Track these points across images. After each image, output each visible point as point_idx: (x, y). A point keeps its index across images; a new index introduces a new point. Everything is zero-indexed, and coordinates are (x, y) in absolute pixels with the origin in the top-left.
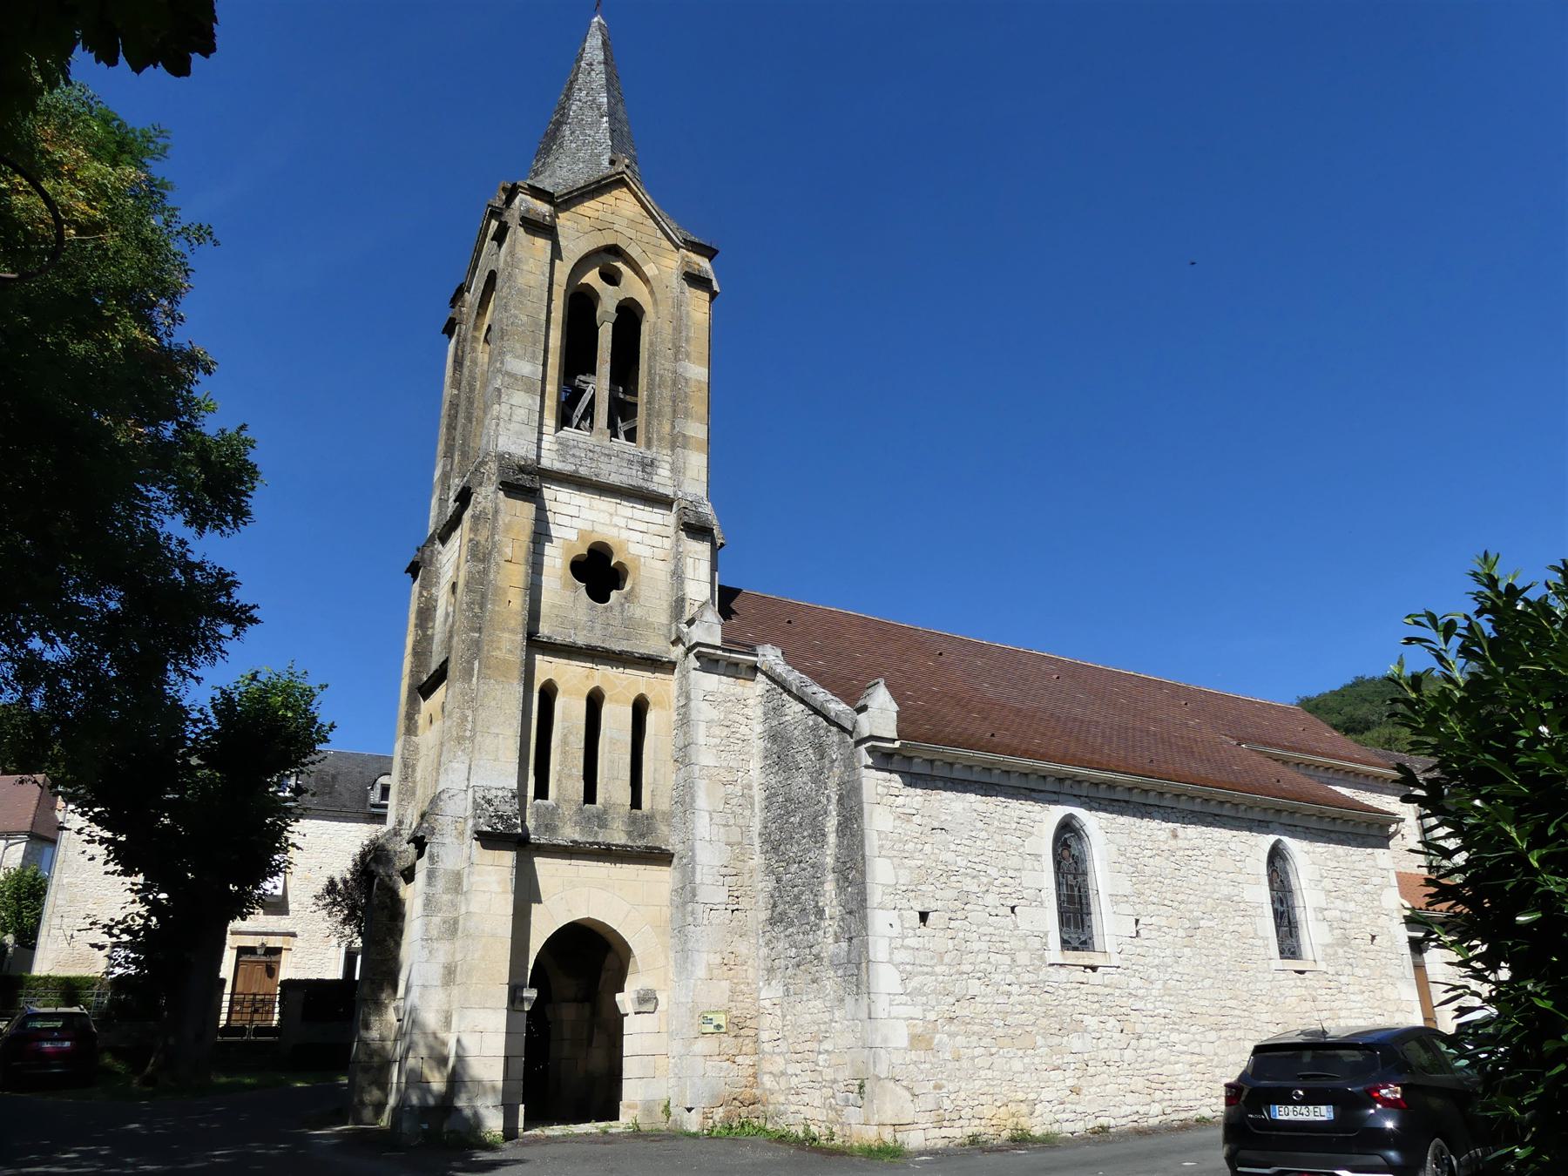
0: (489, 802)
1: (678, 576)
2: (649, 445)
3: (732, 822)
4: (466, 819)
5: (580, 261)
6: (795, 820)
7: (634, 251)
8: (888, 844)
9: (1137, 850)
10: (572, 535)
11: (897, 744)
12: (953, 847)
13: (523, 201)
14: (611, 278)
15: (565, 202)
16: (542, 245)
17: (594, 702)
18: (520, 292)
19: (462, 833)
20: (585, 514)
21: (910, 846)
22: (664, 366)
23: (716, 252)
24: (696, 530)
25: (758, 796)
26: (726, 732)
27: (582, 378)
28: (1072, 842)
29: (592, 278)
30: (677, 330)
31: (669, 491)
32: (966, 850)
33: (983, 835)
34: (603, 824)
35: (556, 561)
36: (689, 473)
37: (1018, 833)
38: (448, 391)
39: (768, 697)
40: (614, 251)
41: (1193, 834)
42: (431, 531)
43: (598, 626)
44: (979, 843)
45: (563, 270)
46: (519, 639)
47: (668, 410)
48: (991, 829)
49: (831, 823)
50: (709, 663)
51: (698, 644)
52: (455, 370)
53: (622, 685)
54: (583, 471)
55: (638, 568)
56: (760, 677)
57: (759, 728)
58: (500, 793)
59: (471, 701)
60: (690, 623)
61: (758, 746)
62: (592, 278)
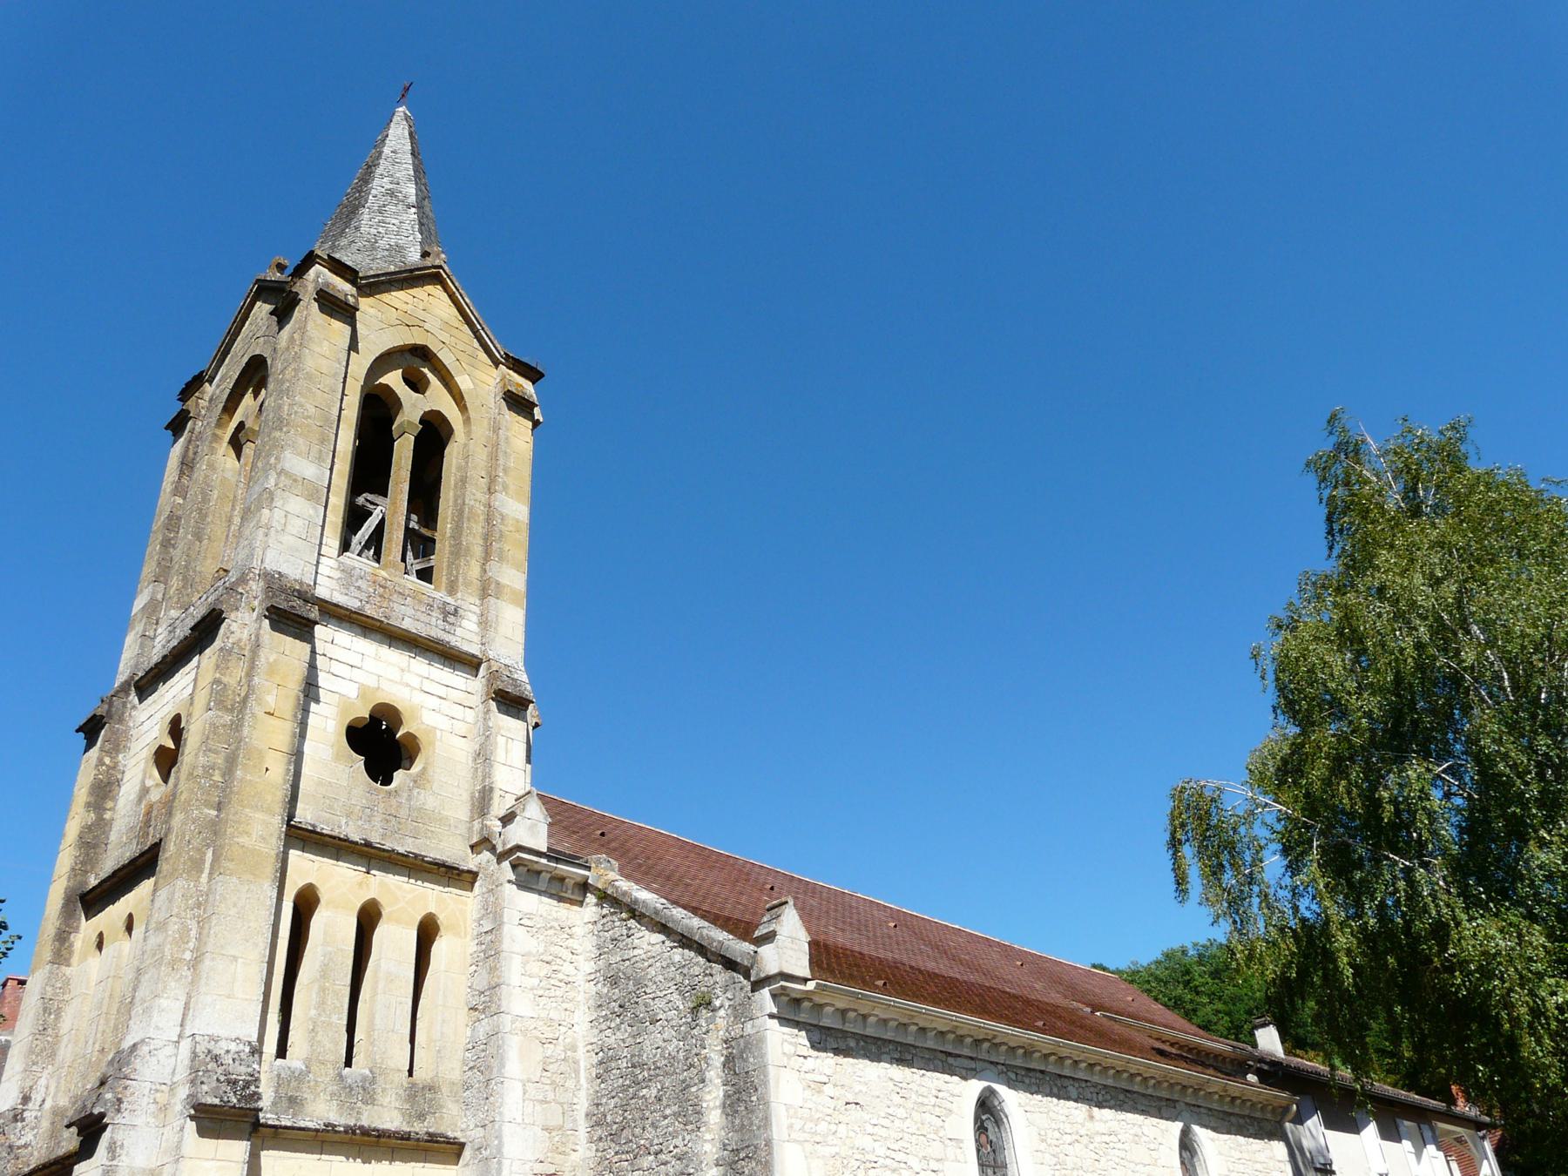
0: (216, 1058)
1: (483, 757)
2: (452, 590)
3: (551, 1096)
4: (172, 1088)
5: (381, 356)
6: (651, 1092)
7: (446, 357)
8: (798, 1124)
9: (1057, 1135)
10: (352, 691)
11: (811, 986)
12: (870, 1129)
13: (319, 274)
14: (416, 384)
15: (370, 285)
16: (340, 329)
17: (368, 919)
18: (309, 377)
19: (164, 1109)
20: (369, 664)
21: (823, 1127)
22: (475, 496)
23: (542, 375)
24: (511, 703)
25: (586, 1061)
26: (546, 969)
27: (370, 497)
28: (989, 1125)
29: (393, 379)
30: (493, 457)
31: (474, 649)
32: (883, 1132)
33: (901, 1112)
34: (370, 1099)
35: (327, 724)
36: (502, 630)
37: (937, 1111)
38: (167, 499)
39: (600, 925)
40: (422, 353)
41: (1108, 1118)
42: (121, 678)
43: (377, 819)
44: (897, 1122)
45: (361, 365)
46: (277, 824)
47: (478, 550)
48: (909, 1104)
49: (713, 1095)
50: (528, 877)
51: (519, 848)
52: (182, 473)
53: (405, 900)
54: (369, 611)
55: (432, 743)
56: (591, 899)
57: (589, 967)
58: (233, 1047)
59: (202, 906)
60: (507, 819)
61: (585, 991)
62: (393, 379)
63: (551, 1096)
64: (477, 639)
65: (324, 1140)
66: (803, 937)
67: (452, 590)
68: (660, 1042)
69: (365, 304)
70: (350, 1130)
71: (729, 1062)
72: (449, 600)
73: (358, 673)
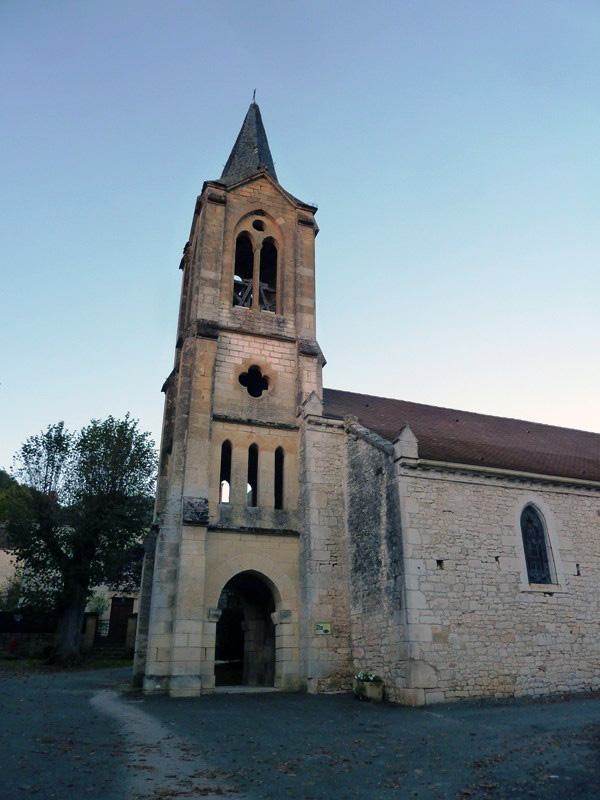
0: (191, 505)
2: (282, 314)
10: (239, 362)
17: (253, 451)
18: (208, 236)
22: (289, 270)
25: (347, 499)
30: (295, 251)
33: (476, 515)
47: (292, 293)
48: (481, 512)
55: (276, 378)
58: (198, 501)
63: (331, 514)
64: (293, 331)
65: (241, 530)
66: (414, 440)
67: (282, 314)
68: (369, 489)
69: (231, 197)
70: (249, 529)
71: (388, 497)
72: (282, 317)
73: (242, 351)
